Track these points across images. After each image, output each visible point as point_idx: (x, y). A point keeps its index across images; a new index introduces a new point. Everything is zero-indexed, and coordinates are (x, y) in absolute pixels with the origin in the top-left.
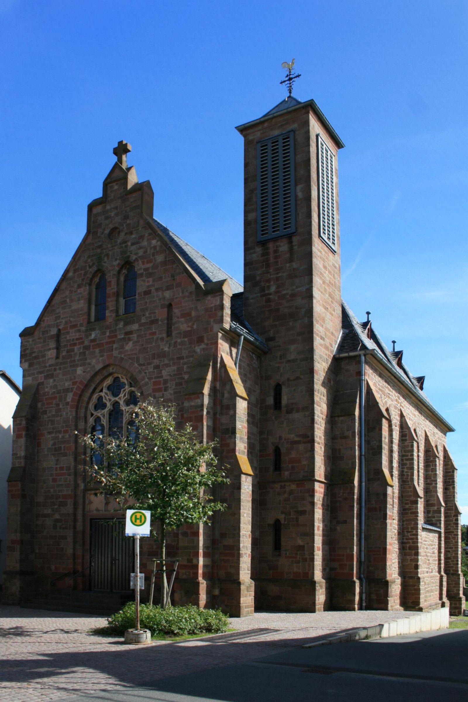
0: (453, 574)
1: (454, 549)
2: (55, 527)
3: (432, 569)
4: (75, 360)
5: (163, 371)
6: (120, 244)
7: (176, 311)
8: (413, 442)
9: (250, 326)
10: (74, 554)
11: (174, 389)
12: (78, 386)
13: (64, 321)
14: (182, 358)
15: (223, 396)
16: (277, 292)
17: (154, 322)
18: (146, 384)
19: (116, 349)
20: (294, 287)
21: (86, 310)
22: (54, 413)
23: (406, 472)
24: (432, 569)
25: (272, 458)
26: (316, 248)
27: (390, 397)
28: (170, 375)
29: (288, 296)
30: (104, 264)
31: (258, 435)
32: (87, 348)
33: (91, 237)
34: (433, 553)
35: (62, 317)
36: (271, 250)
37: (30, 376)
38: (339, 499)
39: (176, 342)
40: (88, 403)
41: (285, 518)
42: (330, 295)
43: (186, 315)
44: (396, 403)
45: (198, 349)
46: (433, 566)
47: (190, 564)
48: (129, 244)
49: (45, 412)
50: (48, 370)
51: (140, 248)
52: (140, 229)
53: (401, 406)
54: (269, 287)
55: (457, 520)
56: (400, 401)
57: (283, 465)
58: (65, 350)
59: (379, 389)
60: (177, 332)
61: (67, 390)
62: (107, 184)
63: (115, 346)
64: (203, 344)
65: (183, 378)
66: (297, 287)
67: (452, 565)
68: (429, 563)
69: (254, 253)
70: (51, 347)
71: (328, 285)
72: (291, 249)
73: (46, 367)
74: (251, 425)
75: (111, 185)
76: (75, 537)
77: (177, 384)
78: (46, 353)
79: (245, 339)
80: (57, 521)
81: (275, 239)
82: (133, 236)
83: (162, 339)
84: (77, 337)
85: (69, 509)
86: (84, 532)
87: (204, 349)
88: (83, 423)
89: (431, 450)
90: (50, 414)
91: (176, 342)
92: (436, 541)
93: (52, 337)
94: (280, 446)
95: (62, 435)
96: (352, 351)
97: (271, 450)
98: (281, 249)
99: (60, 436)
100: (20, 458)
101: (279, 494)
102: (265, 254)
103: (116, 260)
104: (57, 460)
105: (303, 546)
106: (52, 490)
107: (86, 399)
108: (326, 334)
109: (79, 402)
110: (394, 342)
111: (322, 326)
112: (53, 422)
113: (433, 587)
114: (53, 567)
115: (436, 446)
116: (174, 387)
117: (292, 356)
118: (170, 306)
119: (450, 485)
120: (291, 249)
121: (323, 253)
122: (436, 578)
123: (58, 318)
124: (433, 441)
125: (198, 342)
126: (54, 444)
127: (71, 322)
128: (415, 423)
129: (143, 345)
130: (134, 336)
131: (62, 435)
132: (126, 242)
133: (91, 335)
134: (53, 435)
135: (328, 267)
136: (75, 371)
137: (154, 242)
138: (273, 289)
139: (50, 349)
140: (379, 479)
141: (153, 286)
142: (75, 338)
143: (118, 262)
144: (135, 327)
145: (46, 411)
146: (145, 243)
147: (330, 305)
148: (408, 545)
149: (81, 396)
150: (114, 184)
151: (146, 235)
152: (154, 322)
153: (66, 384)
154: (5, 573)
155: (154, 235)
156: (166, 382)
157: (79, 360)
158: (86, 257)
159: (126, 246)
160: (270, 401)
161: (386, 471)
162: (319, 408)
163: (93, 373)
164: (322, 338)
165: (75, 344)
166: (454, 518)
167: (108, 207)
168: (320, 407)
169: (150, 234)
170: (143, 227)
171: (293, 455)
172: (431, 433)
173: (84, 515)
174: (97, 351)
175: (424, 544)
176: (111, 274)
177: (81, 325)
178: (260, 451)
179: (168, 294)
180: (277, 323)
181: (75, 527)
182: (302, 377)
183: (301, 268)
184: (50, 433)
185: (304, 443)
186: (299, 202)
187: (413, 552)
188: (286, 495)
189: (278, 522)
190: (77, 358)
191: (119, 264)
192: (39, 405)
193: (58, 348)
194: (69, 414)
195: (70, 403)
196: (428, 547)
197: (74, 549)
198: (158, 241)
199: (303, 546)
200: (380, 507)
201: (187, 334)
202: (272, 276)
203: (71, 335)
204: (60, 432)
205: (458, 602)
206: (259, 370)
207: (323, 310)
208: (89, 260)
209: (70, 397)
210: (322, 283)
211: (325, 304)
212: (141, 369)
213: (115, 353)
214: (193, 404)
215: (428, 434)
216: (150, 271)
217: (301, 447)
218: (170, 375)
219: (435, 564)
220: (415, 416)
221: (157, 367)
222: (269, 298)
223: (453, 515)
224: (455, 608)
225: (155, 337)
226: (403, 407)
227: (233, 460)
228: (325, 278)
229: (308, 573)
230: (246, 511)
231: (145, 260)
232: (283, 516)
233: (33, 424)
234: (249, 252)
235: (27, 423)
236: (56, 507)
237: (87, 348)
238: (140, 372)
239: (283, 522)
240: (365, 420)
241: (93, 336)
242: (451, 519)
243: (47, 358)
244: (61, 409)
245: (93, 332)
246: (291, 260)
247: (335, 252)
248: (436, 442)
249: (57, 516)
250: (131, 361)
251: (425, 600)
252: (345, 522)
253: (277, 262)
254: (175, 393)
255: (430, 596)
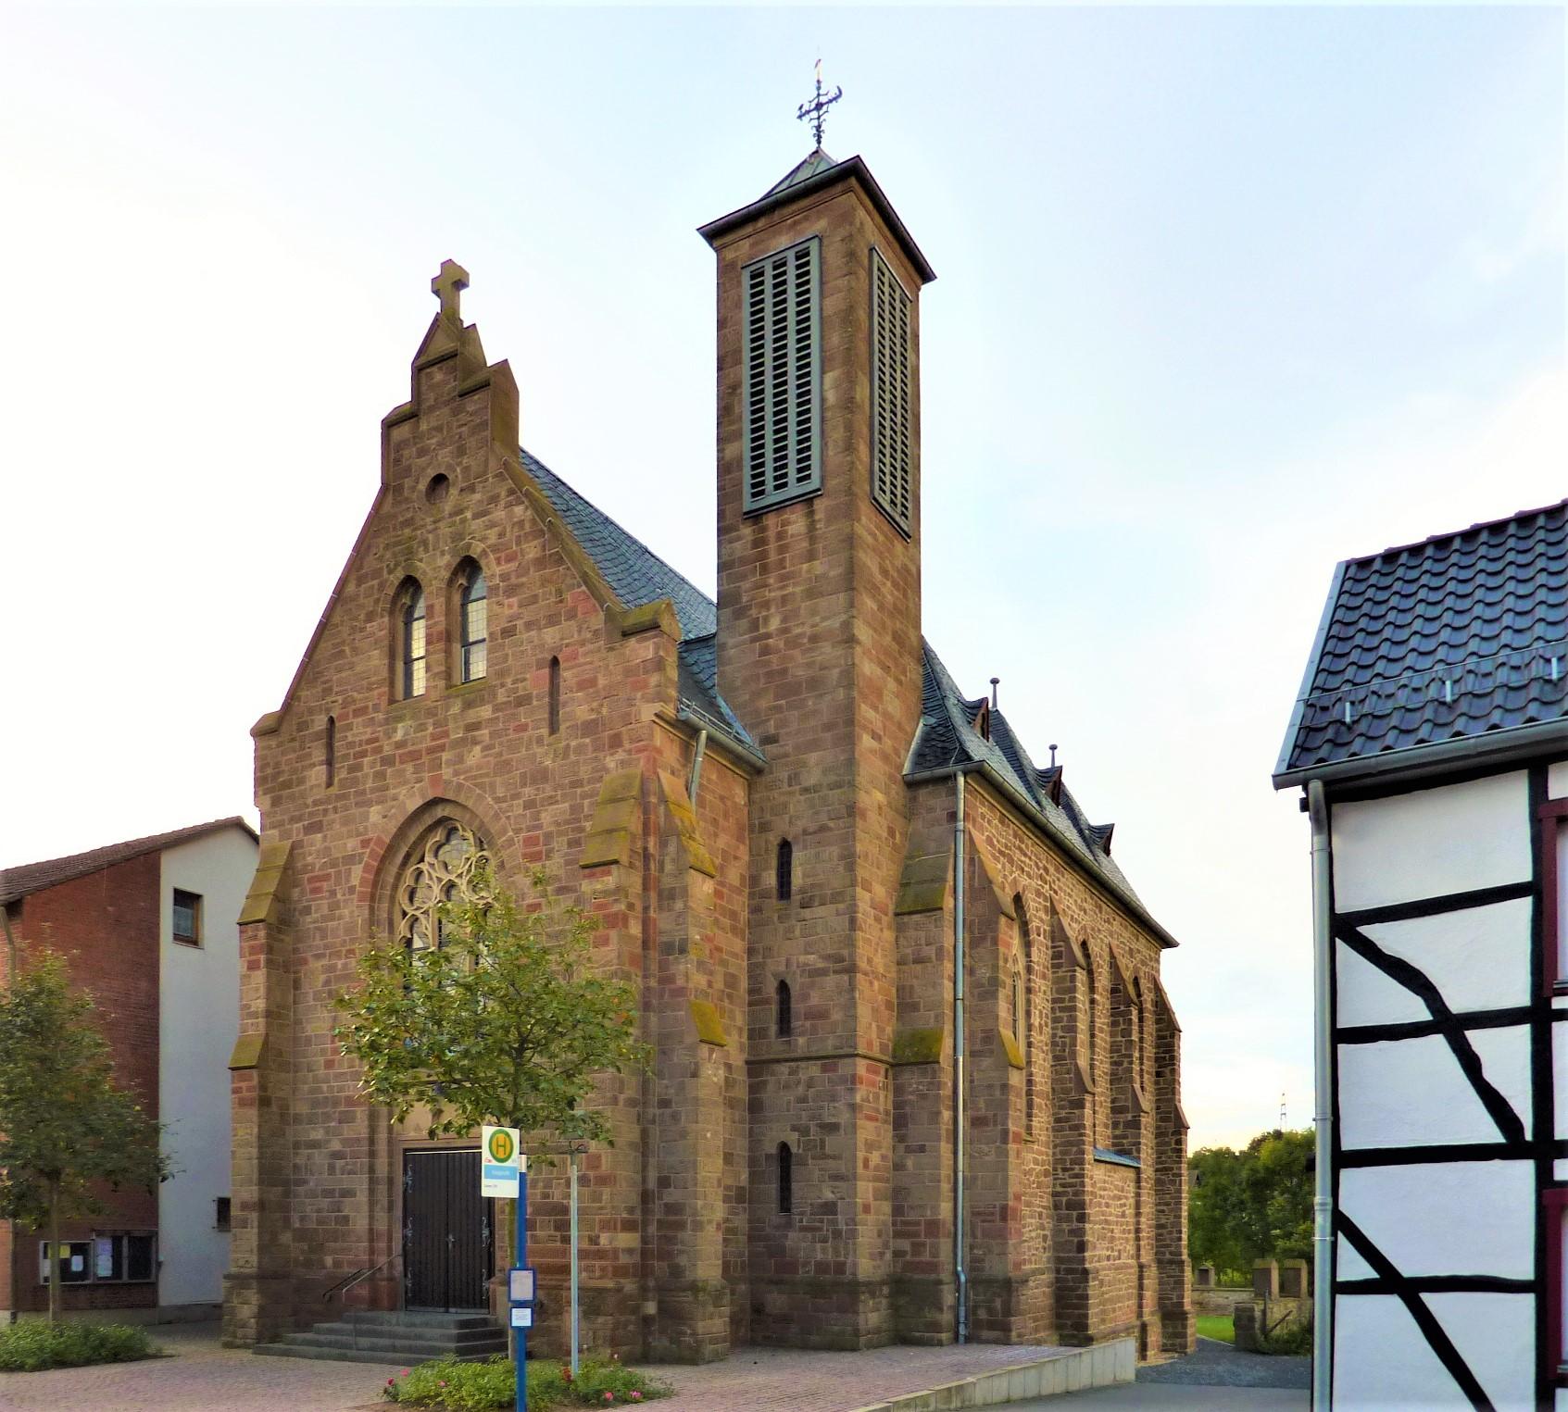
0: (1171, 1262)
1: (1173, 1206)
2: (332, 1169)
3: (1119, 1251)
4: (365, 790)
5: (543, 815)
6: (451, 515)
7: (567, 675)
8: (1075, 971)
9: (728, 710)
10: (371, 1230)
11: (567, 854)
12: (373, 850)
13: (340, 699)
14: (577, 784)
15: (661, 869)
16: (785, 631)
17: (523, 701)
18: (511, 842)
19: (448, 762)
20: (817, 619)
21: (385, 674)
22: (326, 911)
23: (1061, 1037)
24: (1119, 1251)
25: (774, 1008)
26: (863, 526)
27: (1026, 869)
28: (558, 824)
29: (805, 640)
30: (419, 563)
31: (746, 956)
32: (388, 761)
33: (390, 499)
34: (1123, 1215)
35: (335, 689)
36: (771, 534)
37: (274, 828)
38: (910, 1097)
39: (568, 746)
40: (395, 887)
41: (799, 1140)
42: (894, 639)
43: (587, 684)
44: (1040, 883)
45: (611, 762)
46: (1121, 1244)
47: (594, 1247)
48: (469, 515)
49: (307, 910)
50: (309, 813)
51: (492, 525)
52: (490, 479)
53: (1051, 888)
54: (766, 619)
55: (1179, 1142)
56: (1048, 878)
57: (795, 1024)
58: (343, 767)
59: (1001, 852)
60: (568, 724)
61: (350, 859)
62: (422, 367)
63: (445, 756)
64: (620, 750)
65: (581, 830)
66: (824, 619)
67: (1168, 1242)
68: (1113, 1239)
69: (739, 538)
70: (315, 760)
71: (892, 615)
72: (812, 527)
73: (308, 807)
74: (729, 935)
75: (428, 370)
76: (372, 1191)
77: (571, 844)
78: (305, 773)
79: (710, 739)
80: (337, 1155)
81: (780, 506)
82: (477, 496)
83: (540, 740)
84: (368, 736)
85: (360, 1127)
86: (391, 1181)
87: (623, 763)
88: (386, 934)
89: (1121, 987)
90: (318, 915)
91: (568, 746)
92: (1131, 1188)
93: (317, 736)
94: (788, 981)
95: (343, 961)
96: (939, 765)
97: (771, 989)
98: (791, 529)
99: (340, 964)
100: (254, 1015)
101: (787, 1087)
102: (759, 542)
103: (443, 553)
104: (335, 1019)
105: (834, 1204)
106: (325, 1086)
107: (391, 880)
108: (885, 727)
109: (375, 884)
110: (1053, 748)
111: (875, 708)
112: (323, 933)
113: (1120, 1290)
114: (329, 1261)
115: (1136, 982)
116: (565, 849)
117: (812, 778)
118: (555, 662)
119: (1165, 1066)
120: (812, 527)
121: (881, 538)
122: (1129, 1271)
123: (328, 691)
124: (1127, 968)
125: (611, 747)
126: (327, 982)
127: (354, 701)
128: (1084, 928)
129: (500, 754)
130: (484, 733)
131: (343, 961)
132: (461, 512)
133: (395, 731)
134: (325, 962)
135: (891, 572)
136: (366, 817)
137: (519, 510)
138: (775, 624)
139: (314, 765)
140: (992, 1052)
141: (518, 617)
142: (364, 738)
143: (447, 557)
144: (485, 712)
145: (310, 906)
146: (499, 514)
147: (895, 659)
148: (1064, 1199)
149: (379, 872)
150: (435, 369)
151: (503, 494)
152: (523, 701)
153: (349, 845)
154: (227, 1277)
155: (519, 494)
156: (549, 836)
157: (373, 790)
158: (382, 546)
159: (463, 521)
160: (770, 879)
161: (1006, 1033)
162: (867, 896)
163: (402, 820)
164: (876, 737)
165: (363, 754)
166: (1174, 1138)
167: (424, 426)
168: (870, 892)
169: (511, 492)
170: (496, 476)
171: (815, 999)
172: (1124, 949)
173: (390, 1141)
174: (409, 768)
175: (1101, 1196)
176: (433, 589)
177: (376, 708)
178: (751, 992)
179: (550, 636)
180: (783, 702)
181: (372, 1170)
182: (831, 824)
183: (832, 574)
184: (318, 957)
185: (835, 972)
186: (829, 414)
187: (1075, 1213)
188: (801, 1089)
189: (784, 1147)
190: (369, 784)
191: (448, 565)
192: (296, 893)
193: (330, 762)
194: (356, 914)
195: (357, 888)
196: (1111, 1202)
197: (371, 1217)
198: (527, 508)
199: (834, 1204)
200: (995, 1115)
201: (589, 728)
202: (773, 594)
203: (355, 731)
204: (337, 954)
205: (1179, 1323)
206: (746, 811)
207: (879, 671)
208: (388, 555)
209: (357, 874)
210: (875, 608)
211: (882, 658)
212: (500, 809)
213: (446, 773)
214: (599, 887)
215: (1116, 951)
216: (514, 580)
217: (831, 981)
218: (558, 824)
219: (1127, 1240)
220: (1085, 913)
221: (529, 805)
222: (767, 645)
223: (1171, 1131)
224: (1176, 1335)
225: (525, 735)
226: (1056, 892)
227: (683, 1013)
228: (884, 597)
229: (844, 1264)
230: (710, 1127)
231: (503, 555)
232: (795, 1136)
233: (282, 937)
234: (727, 537)
235: (269, 936)
236: (333, 1124)
237: (388, 761)
238: (497, 816)
239: (794, 1150)
240: (964, 919)
241: (399, 735)
242: (1167, 1139)
243: (308, 784)
244: (338, 901)
245: (400, 725)
246: (811, 556)
247: (909, 537)
248: (1136, 969)
249: (336, 1145)
250: (478, 791)
251: (1103, 1321)
252: (922, 1149)
253: (783, 560)
254: (567, 863)
255: (1114, 1310)
